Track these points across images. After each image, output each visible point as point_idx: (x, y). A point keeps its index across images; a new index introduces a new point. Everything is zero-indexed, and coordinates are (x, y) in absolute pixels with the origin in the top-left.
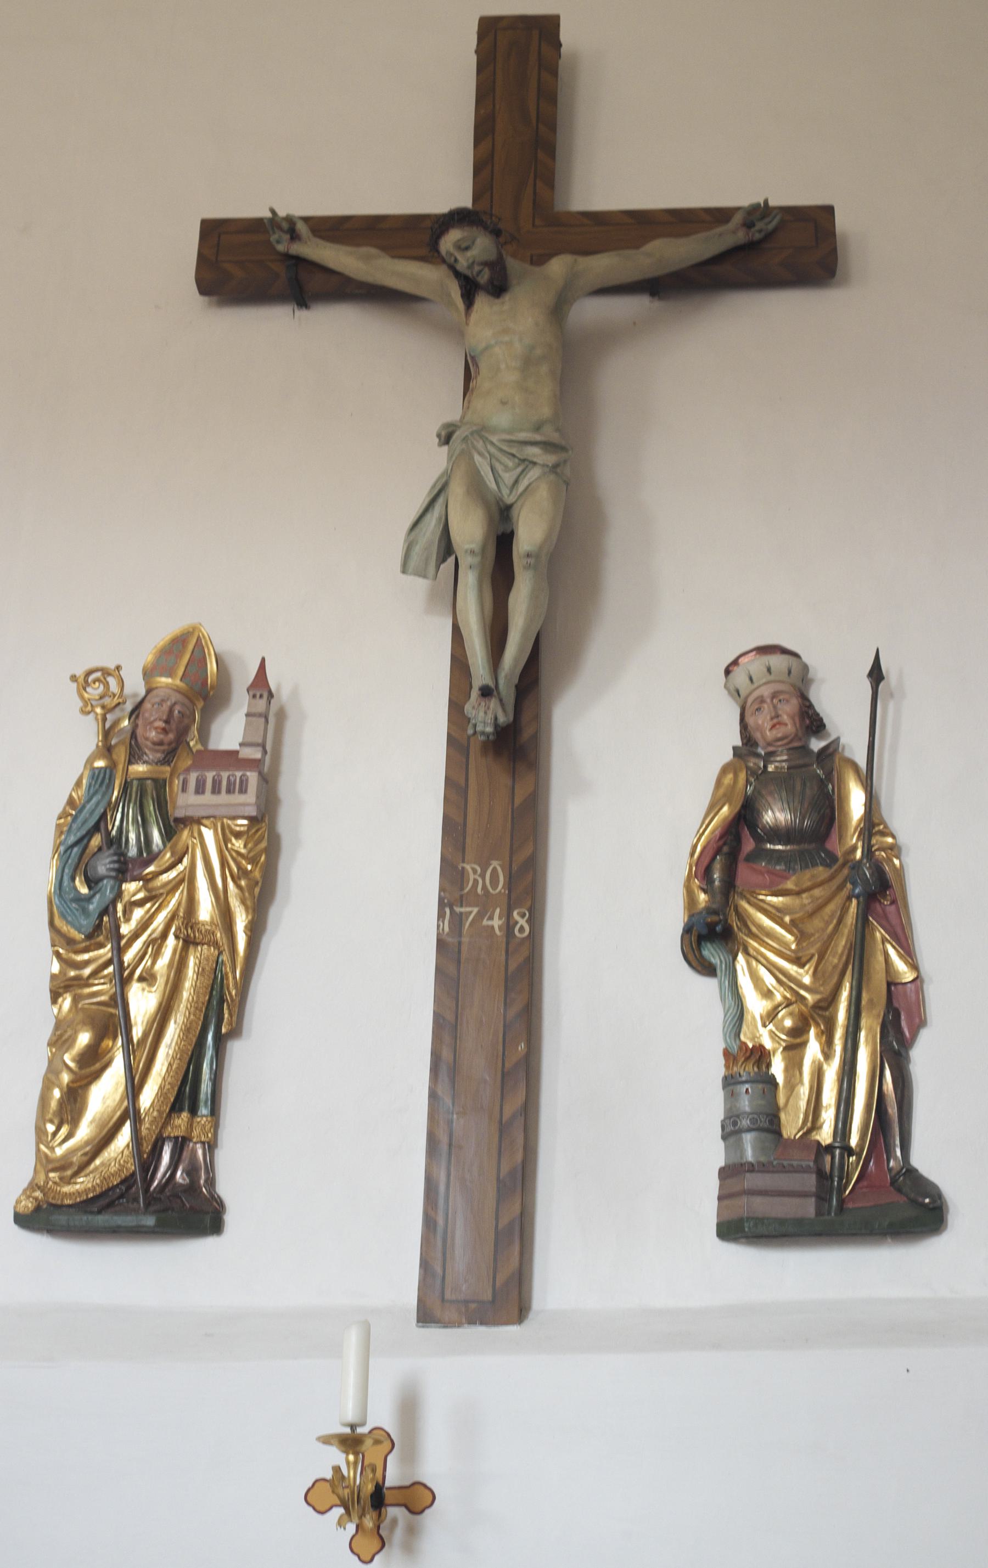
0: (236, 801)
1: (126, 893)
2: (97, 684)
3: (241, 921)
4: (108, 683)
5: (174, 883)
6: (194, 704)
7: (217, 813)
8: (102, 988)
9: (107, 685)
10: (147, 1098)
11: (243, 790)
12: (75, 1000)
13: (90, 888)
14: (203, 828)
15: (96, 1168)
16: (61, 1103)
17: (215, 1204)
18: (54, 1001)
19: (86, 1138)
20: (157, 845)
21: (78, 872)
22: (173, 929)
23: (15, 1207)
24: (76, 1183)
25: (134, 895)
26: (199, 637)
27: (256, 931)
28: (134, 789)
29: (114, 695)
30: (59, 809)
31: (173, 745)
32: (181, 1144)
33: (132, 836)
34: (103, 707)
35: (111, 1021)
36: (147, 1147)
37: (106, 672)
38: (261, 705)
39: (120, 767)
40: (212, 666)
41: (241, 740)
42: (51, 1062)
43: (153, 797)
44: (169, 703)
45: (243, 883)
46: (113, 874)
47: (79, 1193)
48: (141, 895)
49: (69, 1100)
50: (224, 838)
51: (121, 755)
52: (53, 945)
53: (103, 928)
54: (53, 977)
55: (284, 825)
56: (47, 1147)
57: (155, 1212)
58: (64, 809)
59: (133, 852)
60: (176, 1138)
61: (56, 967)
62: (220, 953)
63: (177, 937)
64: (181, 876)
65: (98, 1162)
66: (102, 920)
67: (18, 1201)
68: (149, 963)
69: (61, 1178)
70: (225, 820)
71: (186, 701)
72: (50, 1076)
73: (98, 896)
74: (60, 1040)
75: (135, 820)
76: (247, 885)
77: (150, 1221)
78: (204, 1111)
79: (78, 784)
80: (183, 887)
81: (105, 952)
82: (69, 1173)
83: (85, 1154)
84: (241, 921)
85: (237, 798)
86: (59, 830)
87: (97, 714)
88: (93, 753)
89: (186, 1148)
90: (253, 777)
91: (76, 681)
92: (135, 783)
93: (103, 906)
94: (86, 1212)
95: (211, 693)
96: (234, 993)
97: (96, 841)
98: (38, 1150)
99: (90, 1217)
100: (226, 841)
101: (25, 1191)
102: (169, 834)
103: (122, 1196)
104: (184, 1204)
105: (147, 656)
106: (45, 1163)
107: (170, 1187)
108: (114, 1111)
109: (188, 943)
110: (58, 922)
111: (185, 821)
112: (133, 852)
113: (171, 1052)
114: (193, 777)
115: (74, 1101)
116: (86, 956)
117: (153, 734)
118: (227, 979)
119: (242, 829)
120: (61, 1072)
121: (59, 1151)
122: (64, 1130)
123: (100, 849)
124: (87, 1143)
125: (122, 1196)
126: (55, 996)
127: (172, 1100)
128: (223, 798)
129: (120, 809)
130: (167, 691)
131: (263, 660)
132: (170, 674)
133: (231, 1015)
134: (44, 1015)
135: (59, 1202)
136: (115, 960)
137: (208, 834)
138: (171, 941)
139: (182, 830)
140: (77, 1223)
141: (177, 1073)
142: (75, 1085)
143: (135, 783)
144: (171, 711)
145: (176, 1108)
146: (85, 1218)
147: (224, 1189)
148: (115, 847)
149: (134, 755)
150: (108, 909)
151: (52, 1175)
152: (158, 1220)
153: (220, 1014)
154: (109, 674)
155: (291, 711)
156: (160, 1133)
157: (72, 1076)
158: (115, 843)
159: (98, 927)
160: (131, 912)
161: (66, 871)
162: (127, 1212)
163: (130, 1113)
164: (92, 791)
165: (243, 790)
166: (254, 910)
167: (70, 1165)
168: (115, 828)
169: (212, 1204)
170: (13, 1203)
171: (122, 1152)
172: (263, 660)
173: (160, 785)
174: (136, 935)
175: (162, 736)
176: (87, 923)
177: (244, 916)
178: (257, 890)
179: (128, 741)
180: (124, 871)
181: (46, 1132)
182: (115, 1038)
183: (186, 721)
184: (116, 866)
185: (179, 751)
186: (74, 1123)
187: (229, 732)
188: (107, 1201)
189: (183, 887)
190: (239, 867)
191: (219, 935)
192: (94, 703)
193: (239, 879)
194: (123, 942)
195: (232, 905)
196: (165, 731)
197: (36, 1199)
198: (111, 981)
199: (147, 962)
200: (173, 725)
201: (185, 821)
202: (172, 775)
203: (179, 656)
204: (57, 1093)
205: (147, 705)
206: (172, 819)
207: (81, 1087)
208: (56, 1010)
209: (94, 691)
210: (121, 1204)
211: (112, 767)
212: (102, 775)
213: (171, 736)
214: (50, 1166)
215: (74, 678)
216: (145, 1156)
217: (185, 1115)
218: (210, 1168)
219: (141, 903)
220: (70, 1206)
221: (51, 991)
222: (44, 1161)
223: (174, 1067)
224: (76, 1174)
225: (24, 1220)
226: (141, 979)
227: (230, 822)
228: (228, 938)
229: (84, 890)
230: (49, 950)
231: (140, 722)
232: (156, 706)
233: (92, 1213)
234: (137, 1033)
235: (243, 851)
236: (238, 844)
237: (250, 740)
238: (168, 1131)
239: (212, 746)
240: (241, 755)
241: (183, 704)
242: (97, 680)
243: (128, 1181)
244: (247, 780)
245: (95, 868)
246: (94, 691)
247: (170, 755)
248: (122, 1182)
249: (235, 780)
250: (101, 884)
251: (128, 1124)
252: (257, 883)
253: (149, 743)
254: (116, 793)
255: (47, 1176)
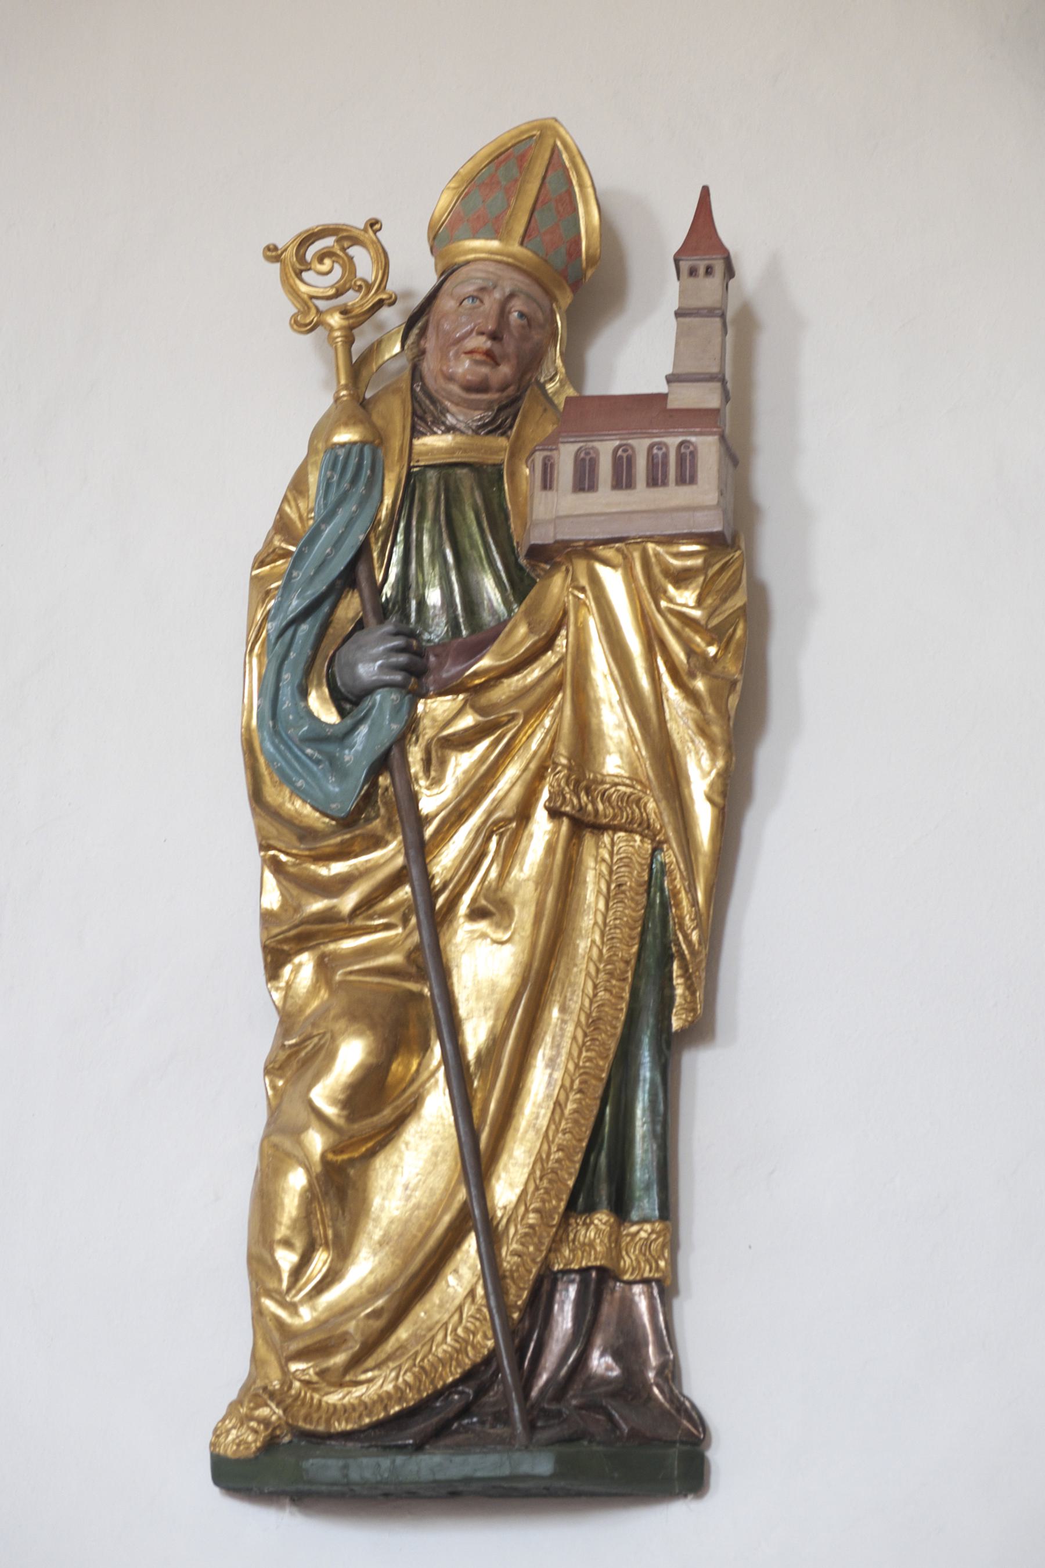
0: (674, 503)
1: (426, 722)
2: (328, 262)
3: (700, 772)
4: (351, 259)
5: (539, 691)
6: (553, 299)
7: (631, 529)
8: (389, 940)
9: (349, 265)
10: (506, 1189)
11: (687, 476)
12: (325, 966)
13: (342, 713)
14: (600, 569)
15: (402, 1348)
16: (309, 1199)
17: (685, 1423)
18: (273, 972)
19: (371, 1280)
20: (494, 612)
21: (314, 677)
22: (545, 795)
23: (213, 1445)
24: (357, 1383)
25: (448, 723)
26: (554, 149)
27: (733, 795)
28: (430, 488)
29: (369, 287)
30: (257, 546)
31: (511, 390)
32: (598, 1283)
33: (434, 597)
34: (345, 312)
35: (411, 1010)
36: (519, 1296)
37: (346, 237)
38: (708, 290)
39: (396, 443)
40: (588, 217)
41: (669, 370)
42: (274, 1111)
43: (469, 504)
44: (497, 295)
45: (700, 685)
46: (398, 677)
47: (366, 1407)
48: (468, 720)
49: (325, 1194)
50: (650, 586)
51: (395, 414)
52: (264, 847)
53: (378, 802)
54: (267, 918)
55: (773, 560)
56: (283, 1304)
57: (551, 1443)
58: (269, 542)
59: (438, 630)
60: (584, 1271)
61: (272, 898)
62: (657, 848)
63: (554, 813)
64: (556, 674)
65: (403, 1333)
66: (375, 784)
67: (218, 1433)
68: (493, 874)
69: (322, 1373)
70: (650, 546)
71: (536, 291)
72: (276, 1139)
73: (364, 730)
74: (297, 1056)
75: (437, 553)
76: (711, 691)
77: (543, 1465)
78: (647, 1204)
79: (298, 486)
80: (564, 700)
81: (389, 855)
82: (339, 1359)
83: (376, 1314)
84: (700, 772)
85: (674, 495)
86: (259, 587)
87: (331, 329)
88: (327, 415)
89: (607, 1297)
90: (707, 448)
91: (277, 259)
92: (432, 475)
93: (379, 749)
94: (387, 1449)
95: (589, 273)
96: (695, 936)
97: (350, 607)
98: (259, 1312)
99: (400, 1459)
100: (657, 592)
101: (233, 1407)
102: (519, 585)
103: (466, 1411)
104: (615, 1426)
105: (440, 200)
106: (275, 1338)
107: (577, 1386)
108: (435, 1218)
109: (581, 826)
110: (278, 796)
111: (550, 555)
112: (438, 630)
113: (558, 1075)
114: (566, 457)
115: (340, 1188)
116: (338, 868)
117: (464, 367)
118: (678, 905)
119: (689, 563)
120: (304, 1128)
121: (306, 1315)
122: (321, 1261)
123: (360, 625)
124: (375, 1292)
125: (466, 1411)
126: (276, 958)
127: (571, 1183)
128: (641, 496)
129: (400, 538)
130: (492, 268)
131: (705, 192)
132: (495, 229)
133: (690, 988)
134: (248, 1014)
135: (321, 1428)
136: (415, 872)
137: (613, 580)
138: (542, 825)
139: (549, 574)
140: (368, 1475)
141: (576, 1122)
142: (340, 1158)
143: (432, 475)
144: (503, 312)
145: (579, 1203)
146: (385, 1462)
147: (703, 1386)
148: (394, 619)
149: (424, 415)
150: (387, 760)
151: (294, 1367)
152: (559, 1461)
153: (660, 997)
154: (355, 241)
155: (766, 313)
156: (546, 1264)
157: (333, 1137)
158: (398, 610)
159: (368, 799)
160: (443, 763)
161: (286, 676)
162: (483, 1444)
163: (474, 1217)
164: (333, 497)
165: (687, 476)
166: (729, 748)
167: (344, 1339)
168: (392, 578)
169: (678, 1425)
170: (209, 1437)
171: (460, 1309)
172: (705, 192)
173: (490, 477)
174: (457, 815)
175: (484, 370)
176: (343, 793)
177: (706, 762)
178: (733, 701)
179: (405, 385)
180: (417, 674)
181: (274, 1269)
182: (425, 1048)
183: (536, 336)
184: (402, 659)
185: (525, 404)
186: (343, 1252)
187: (637, 354)
188: (435, 1420)
189: (564, 700)
190: (690, 652)
191: (651, 805)
192: (322, 304)
193: (692, 675)
194: (429, 831)
195: (675, 737)
196: (491, 358)
197: (265, 1422)
198: (405, 921)
199: (490, 870)
200: (510, 345)
201: (550, 555)
202: (513, 454)
203: (513, 189)
204: (297, 1180)
205: (446, 303)
206: (522, 551)
207: (351, 1161)
208: (278, 996)
209: (319, 281)
210: (466, 1429)
211: (375, 443)
212: (353, 461)
213: (505, 370)
214: (294, 1346)
215: (273, 253)
216: (516, 1316)
217: (602, 1218)
218: (667, 1339)
219: (465, 741)
220: (346, 1436)
221: (265, 948)
222: (276, 1336)
223: (570, 1106)
224: (356, 1362)
225: (233, 1475)
226: (477, 913)
227: (660, 549)
228: (672, 810)
229: (329, 716)
230: (254, 856)
231: (430, 344)
232: (467, 303)
233: (402, 1449)
234: (475, 1036)
235: (697, 614)
236: (685, 598)
237: (690, 367)
238: (565, 1258)
239: (593, 388)
240: (672, 404)
241: (529, 297)
242: (321, 257)
243: (480, 1375)
244: (693, 454)
245: (353, 666)
246: (319, 281)
247: (503, 416)
248: (467, 1377)
249: (666, 456)
250: (367, 703)
251: (471, 1244)
252: (734, 683)
253: (455, 388)
254: (388, 501)
255: (285, 1371)
